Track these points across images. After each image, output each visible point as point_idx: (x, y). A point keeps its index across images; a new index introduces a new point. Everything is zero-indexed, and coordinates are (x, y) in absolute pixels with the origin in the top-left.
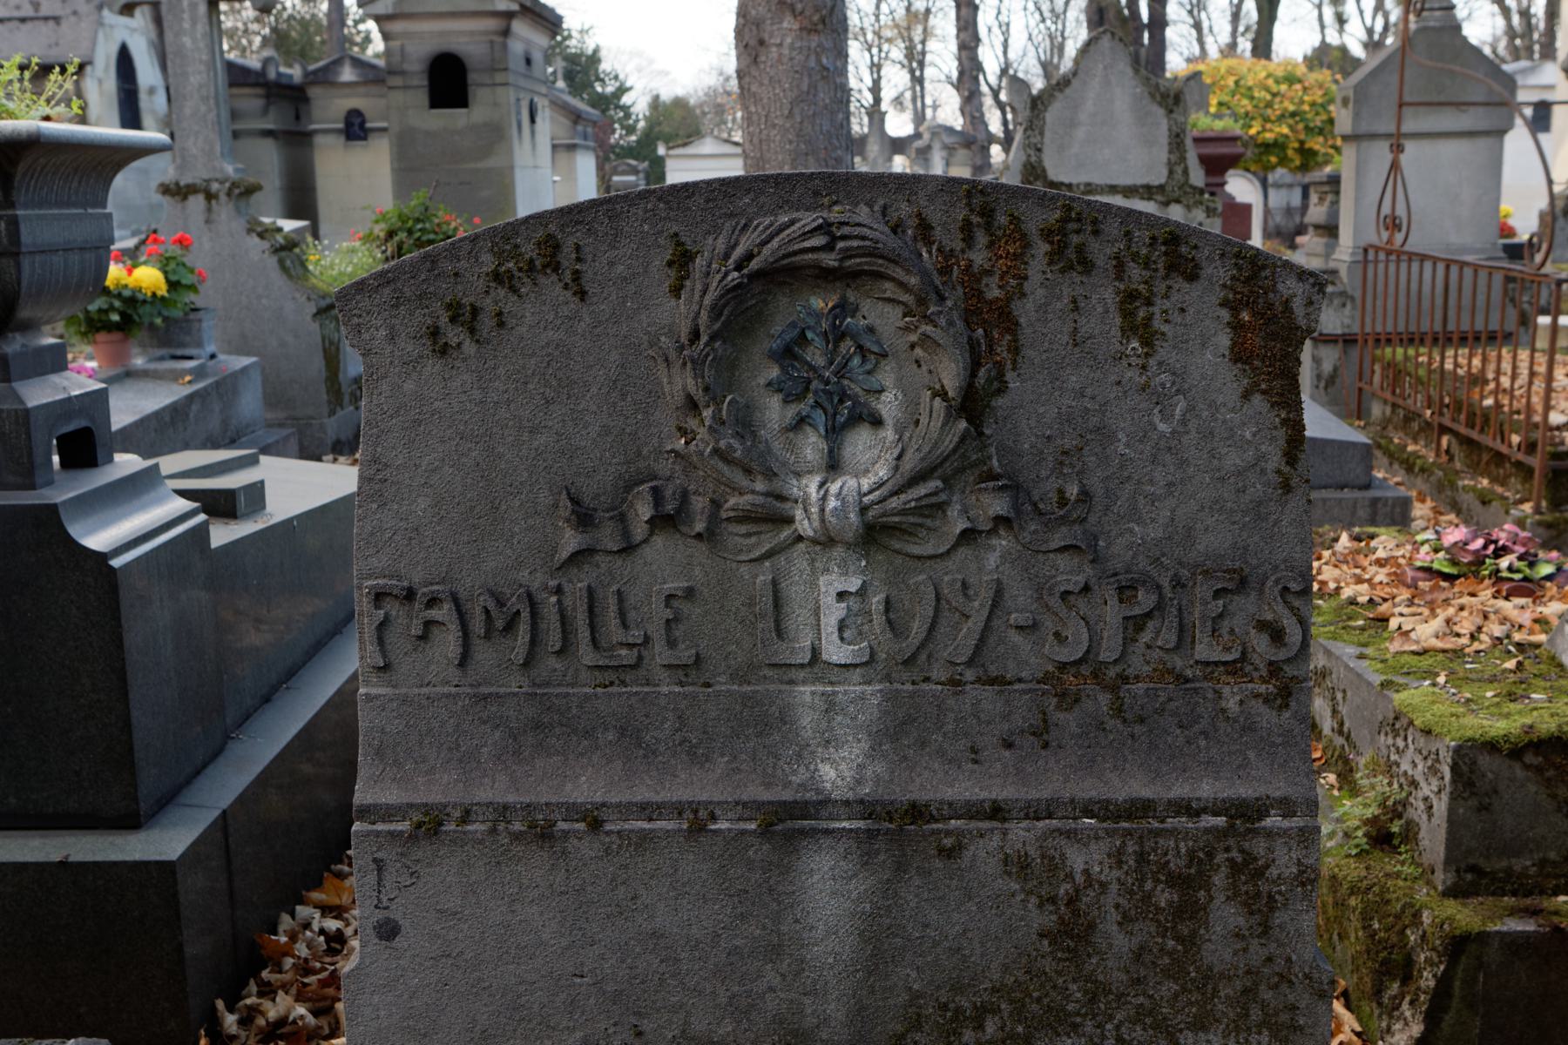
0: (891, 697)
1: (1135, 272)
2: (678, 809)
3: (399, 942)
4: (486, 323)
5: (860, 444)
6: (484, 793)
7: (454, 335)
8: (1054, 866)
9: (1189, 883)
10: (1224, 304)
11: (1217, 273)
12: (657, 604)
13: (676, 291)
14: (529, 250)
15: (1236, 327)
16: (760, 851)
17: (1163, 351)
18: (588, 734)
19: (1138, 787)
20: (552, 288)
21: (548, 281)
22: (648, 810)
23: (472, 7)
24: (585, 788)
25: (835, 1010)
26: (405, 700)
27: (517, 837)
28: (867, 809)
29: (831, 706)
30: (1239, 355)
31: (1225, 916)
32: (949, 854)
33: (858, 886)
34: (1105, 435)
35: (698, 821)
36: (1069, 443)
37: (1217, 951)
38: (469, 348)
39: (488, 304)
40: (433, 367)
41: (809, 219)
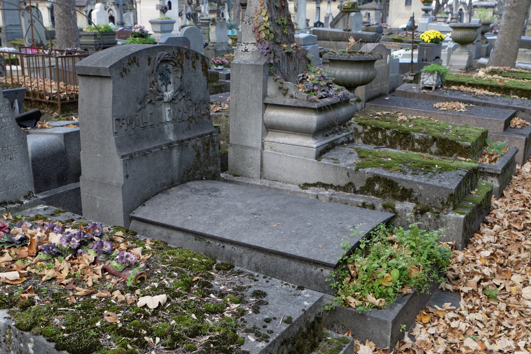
0: (174, 125)
1: (193, 59)
2: (158, 147)
3: (129, 178)
4: (127, 71)
5: (170, 87)
6: (136, 150)
7: (124, 74)
8: (196, 145)
9: (208, 145)
10: (417, 27)
11: (200, 58)
12: (149, 115)
13: (149, 64)
14: (132, 59)
15: (202, 66)
16: (168, 151)
17: (196, 70)
18: (143, 138)
19: (200, 133)
20: (135, 65)
21: (134, 64)
22: (155, 148)
23: (8, 1)
24: (147, 147)
25: (176, 174)
26: (120, 137)
27: (142, 156)
28: (178, 142)
29: (168, 128)
30: (203, 70)
31: (211, 149)
32: (187, 146)
33: (178, 154)
34: (191, 82)
35: (160, 147)
36: (188, 84)
37: (211, 154)
38: (125, 76)
39: (127, 68)
40: (121, 79)
41: (165, 53)
